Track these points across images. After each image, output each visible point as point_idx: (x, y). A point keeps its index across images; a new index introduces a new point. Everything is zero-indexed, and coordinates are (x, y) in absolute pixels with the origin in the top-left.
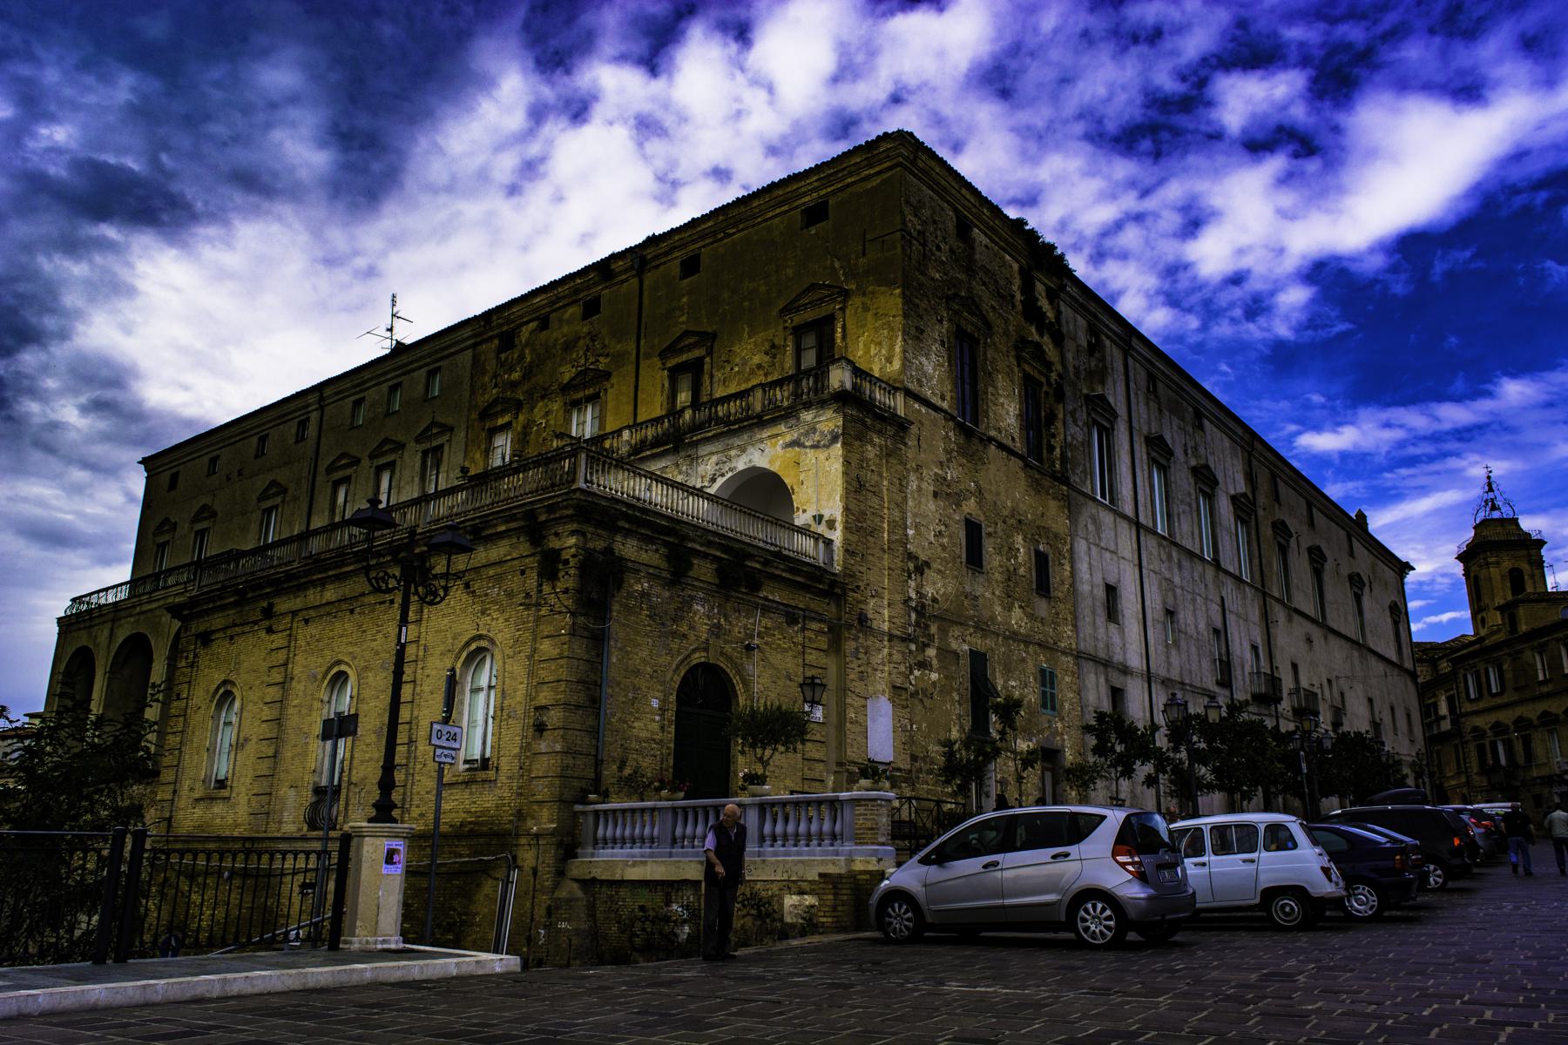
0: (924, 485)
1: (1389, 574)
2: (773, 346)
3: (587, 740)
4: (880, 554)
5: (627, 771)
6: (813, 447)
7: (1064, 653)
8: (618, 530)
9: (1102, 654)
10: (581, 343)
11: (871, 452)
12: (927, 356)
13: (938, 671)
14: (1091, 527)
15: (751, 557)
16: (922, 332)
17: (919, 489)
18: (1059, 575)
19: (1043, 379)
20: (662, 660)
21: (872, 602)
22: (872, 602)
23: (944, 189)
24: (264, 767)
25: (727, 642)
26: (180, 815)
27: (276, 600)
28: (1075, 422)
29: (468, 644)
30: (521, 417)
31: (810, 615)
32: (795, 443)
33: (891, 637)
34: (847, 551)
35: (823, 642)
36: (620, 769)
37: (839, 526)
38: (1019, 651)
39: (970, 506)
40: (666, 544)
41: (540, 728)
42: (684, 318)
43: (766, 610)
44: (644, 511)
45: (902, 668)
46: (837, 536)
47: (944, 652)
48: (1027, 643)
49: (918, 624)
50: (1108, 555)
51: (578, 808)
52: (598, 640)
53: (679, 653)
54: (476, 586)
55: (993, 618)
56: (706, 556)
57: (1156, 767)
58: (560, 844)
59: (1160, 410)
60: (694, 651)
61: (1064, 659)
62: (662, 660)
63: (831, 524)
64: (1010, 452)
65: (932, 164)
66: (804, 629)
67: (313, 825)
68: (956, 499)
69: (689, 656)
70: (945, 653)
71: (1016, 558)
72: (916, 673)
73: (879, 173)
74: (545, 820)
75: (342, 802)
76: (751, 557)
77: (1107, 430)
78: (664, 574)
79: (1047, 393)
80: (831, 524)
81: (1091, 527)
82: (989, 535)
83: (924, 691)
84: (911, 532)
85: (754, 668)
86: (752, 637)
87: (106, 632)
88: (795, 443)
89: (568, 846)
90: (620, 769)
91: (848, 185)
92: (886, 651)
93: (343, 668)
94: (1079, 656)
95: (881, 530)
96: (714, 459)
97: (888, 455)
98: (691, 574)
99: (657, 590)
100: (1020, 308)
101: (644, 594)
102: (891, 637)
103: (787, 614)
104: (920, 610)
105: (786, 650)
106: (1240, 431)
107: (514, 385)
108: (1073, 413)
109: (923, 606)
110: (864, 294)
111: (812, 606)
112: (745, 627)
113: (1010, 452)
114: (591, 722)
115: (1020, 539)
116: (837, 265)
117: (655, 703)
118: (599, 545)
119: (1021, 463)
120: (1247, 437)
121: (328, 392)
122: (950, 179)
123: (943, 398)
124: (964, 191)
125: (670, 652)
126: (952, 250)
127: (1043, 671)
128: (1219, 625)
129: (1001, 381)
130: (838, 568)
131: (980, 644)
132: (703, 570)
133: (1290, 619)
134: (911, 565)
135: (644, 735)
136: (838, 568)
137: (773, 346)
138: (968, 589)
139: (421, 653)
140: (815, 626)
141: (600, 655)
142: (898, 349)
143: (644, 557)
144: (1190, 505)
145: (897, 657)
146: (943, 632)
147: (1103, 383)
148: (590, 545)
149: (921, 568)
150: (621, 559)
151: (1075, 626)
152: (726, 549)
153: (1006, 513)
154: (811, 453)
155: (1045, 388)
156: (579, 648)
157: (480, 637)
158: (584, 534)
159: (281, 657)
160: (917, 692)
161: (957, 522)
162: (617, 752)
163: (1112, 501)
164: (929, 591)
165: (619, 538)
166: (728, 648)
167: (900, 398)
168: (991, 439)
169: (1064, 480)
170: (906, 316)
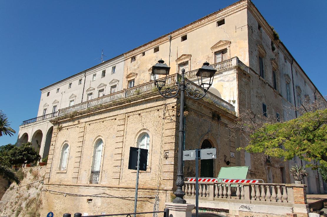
0: (254, 94)
2: (208, 57)
5: (190, 171)
6: (227, 81)
10: (154, 58)
17: (253, 94)
24: (77, 165)
26: (52, 177)
29: (63, 143)
36: (188, 170)
39: (264, 100)
41: (166, 157)
42: (182, 51)
57: (41, 163)
63: (234, 102)
64: (271, 87)
67: (91, 182)
68: (260, 98)
75: (100, 176)
77: (288, 83)
80: (234, 102)
84: (252, 106)
87: (31, 130)
90: (188, 170)
93: (100, 137)
106: (313, 87)
110: (236, 42)
113: (271, 87)
120: (314, 89)
137: (208, 57)
139: (125, 134)
157: (144, 129)
159: (82, 134)
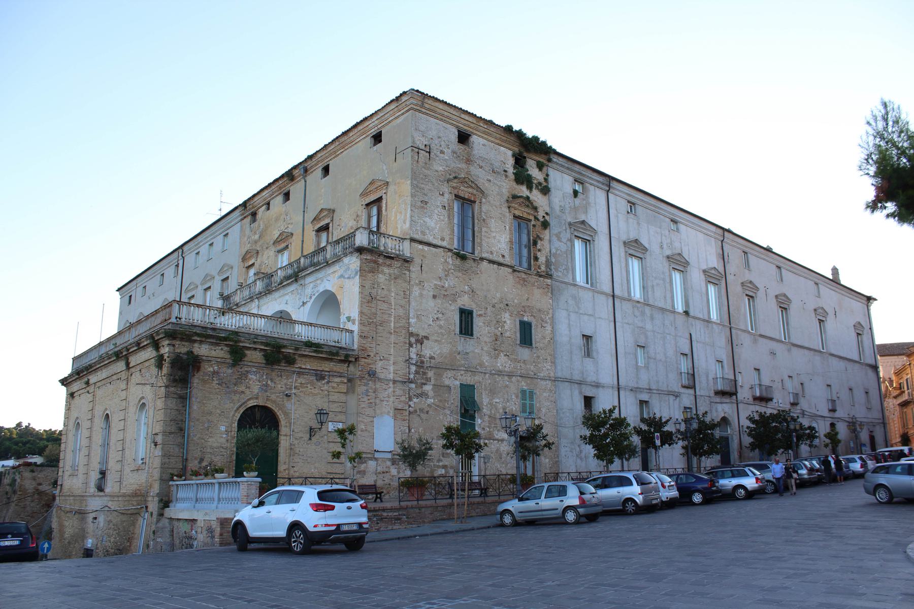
0: (425, 292)
1: (858, 306)
2: (357, 216)
3: (177, 449)
4: (388, 335)
7: (542, 379)
8: (195, 341)
9: (577, 377)
11: (381, 278)
12: (430, 217)
13: (433, 398)
14: (571, 302)
15: (285, 347)
16: (426, 203)
17: (421, 295)
18: (536, 334)
19: (532, 218)
20: (227, 406)
21: (380, 364)
22: (380, 364)
23: (447, 117)
25: (272, 393)
27: (90, 377)
28: (559, 239)
30: (259, 260)
31: (332, 374)
32: (342, 276)
33: (395, 382)
34: (361, 336)
35: (343, 388)
37: (357, 323)
38: (502, 381)
40: (227, 345)
43: (300, 374)
44: (214, 329)
45: (403, 398)
46: (355, 328)
47: (437, 387)
48: (510, 376)
49: (417, 372)
50: (586, 317)
51: (171, 483)
52: (183, 399)
53: (239, 401)
54: (143, 371)
55: (481, 364)
56: (255, 349)
58: (161, 501)
59: (638, 224)
60: (249, 400)
61: (543, 383)
62: (227, 406)
65: (437, 104)
66: (328, 382)
69: (245, 402)
70: (439, 388)
71: (503, 327)
72: (415, 400)
73: (403, 114)
74: (156, 488)
76: (285, 347)
78: (228, 361)
79: (534, 226)
81: (571, 302)
82: (480, 315)
83: (421, 410)
85: (290, 405)
86: (291, 389)
88: (342, 276)
89: (165, 503)
91: (390, 122)
92: (391, 390)
94: (556, 380)
95: (389, 322)
96: (312, 285)
97: (395, 278)
98: (246, 359)
99: (224, 369)
100: (513, 177)
101: (214, 373)
102: (395, 382)
103: (316, 375)
104: (420, 365)
105: (316, 395)
107: (256, 242)
108: (558, 236)
109: (422, 362)
111: (335, 369)
112: (286, 384)
114: (179, 440)
115: (507, 315)
116: (384, 168)
117: (223, 428)
118: (184, 350)
119: (510, 270)
121: (186, 248)
122: (452, 111)
123: (443, 239)
124: (463, 116)
125: (233, 401)
126: (454, 152)
127: (523, 392)
128: (687, 350)
129: (493, 223)
130: (356, 347)
131: (468, 379)
132: (255, 356)
133: (755, 342)
134: (413, 340)
135: (215, 445)
136: (356, 347)
138: (460, 348)
140: (338, 380)
141: (185, 406)
142: (408, 216)
143: (213, 353)
144: (664, 280)
145: (398, 392)
146: (439, 376)
147: (586, 212)
148: (178, 351)
149: (420, 341)
150: (197, 356)
151: (553, 363)
152: (267, 344)
153: (494, 301)
154: (347, 280)
155: (533, 223)
156: (172, 403)
158: (174, 345)
160: (416, 411)
161: (453, 311)
162: (198, 454)
163: (592, 285)
164: (427, 352)
165: (196, 345)
166: (273, 397)
167: (407, 244)
168: (482, 259)
169: (549, 276)
170: (413, 196)
